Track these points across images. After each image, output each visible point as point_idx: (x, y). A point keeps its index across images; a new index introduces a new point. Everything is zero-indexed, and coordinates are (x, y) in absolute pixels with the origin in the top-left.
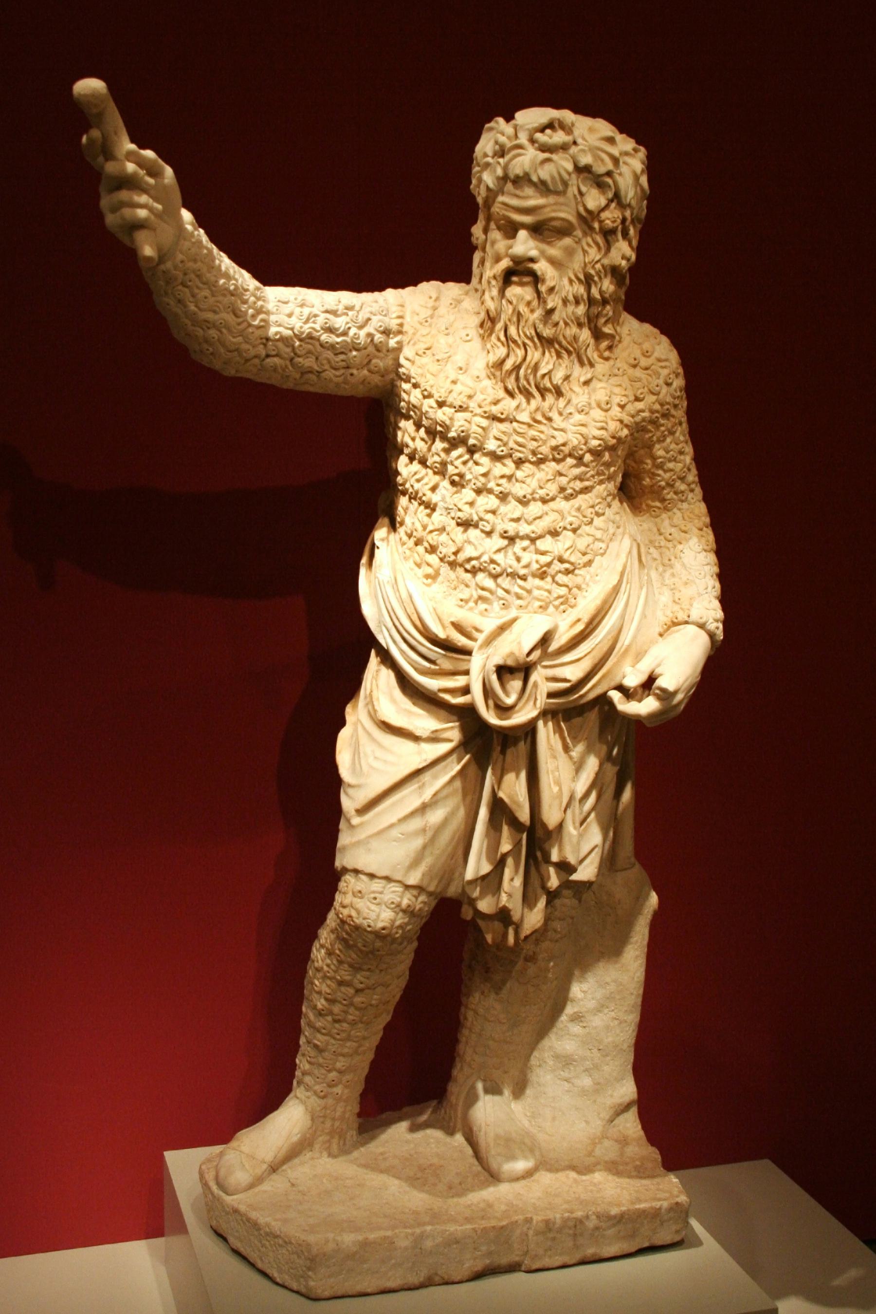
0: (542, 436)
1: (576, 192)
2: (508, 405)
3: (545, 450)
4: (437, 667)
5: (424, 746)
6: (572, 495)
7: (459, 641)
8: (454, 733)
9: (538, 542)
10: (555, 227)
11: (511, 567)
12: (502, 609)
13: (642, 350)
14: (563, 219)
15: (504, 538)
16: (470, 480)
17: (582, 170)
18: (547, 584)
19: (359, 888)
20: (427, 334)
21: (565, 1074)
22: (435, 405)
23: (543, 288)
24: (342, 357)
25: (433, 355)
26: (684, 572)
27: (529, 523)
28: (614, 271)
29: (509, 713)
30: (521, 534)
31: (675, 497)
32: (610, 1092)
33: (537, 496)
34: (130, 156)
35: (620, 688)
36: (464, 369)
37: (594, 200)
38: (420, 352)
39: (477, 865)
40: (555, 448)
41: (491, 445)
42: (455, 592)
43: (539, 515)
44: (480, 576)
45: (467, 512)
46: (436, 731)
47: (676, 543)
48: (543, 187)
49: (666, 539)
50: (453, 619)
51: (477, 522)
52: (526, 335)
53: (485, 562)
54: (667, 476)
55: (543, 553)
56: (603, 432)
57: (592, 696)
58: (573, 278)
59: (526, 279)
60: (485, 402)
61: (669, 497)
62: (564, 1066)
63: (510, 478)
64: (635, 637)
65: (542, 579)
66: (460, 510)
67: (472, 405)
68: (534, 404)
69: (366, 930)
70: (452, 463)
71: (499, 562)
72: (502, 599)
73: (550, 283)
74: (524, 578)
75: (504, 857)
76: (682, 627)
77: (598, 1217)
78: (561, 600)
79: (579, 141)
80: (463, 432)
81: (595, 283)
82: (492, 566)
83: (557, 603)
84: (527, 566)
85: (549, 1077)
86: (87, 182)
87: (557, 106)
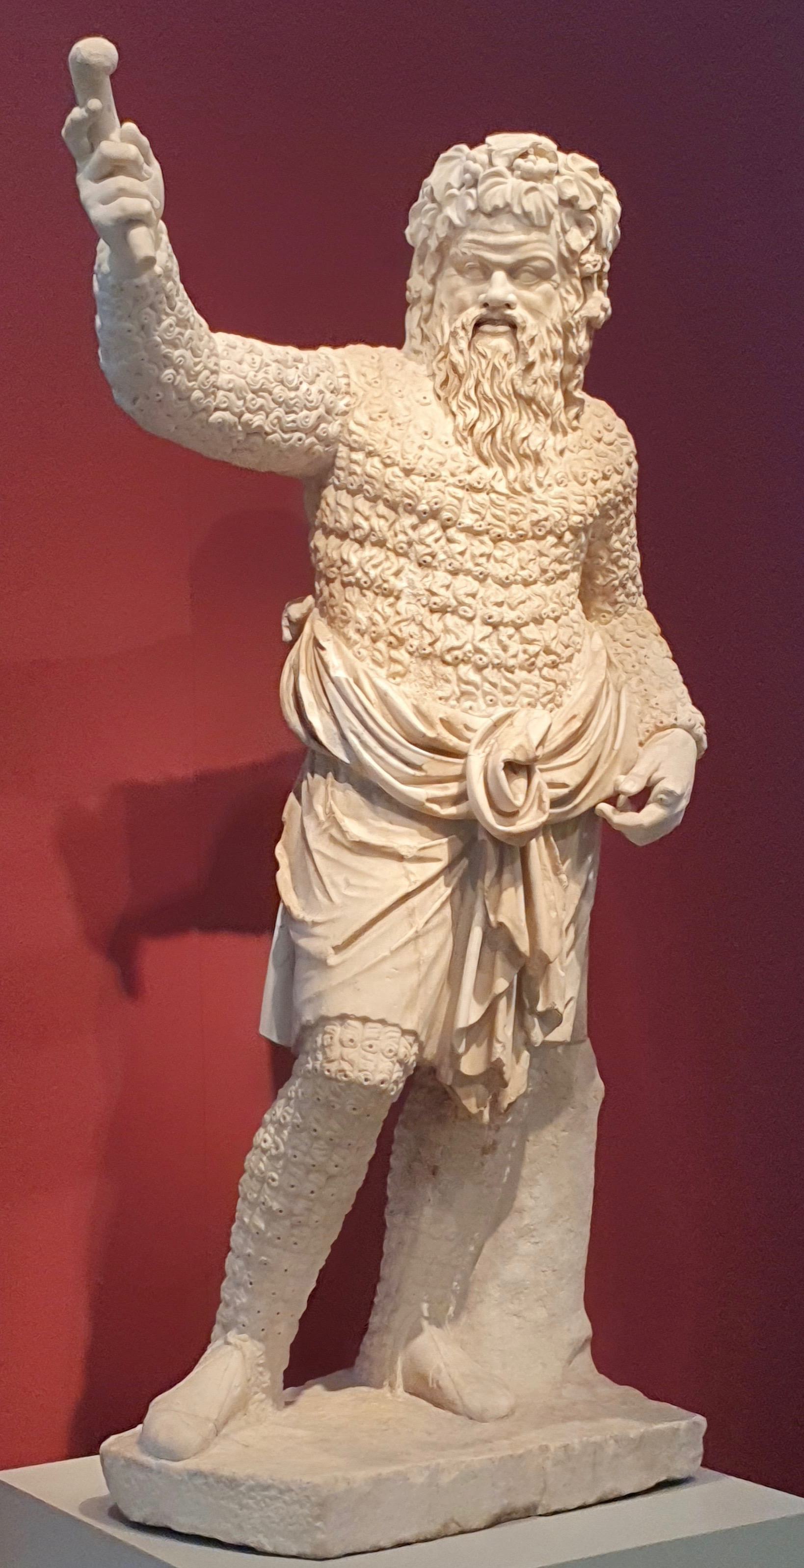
0: (523, 509)
1: (559, 229)
2: (484, 473)
3: (526, 525)
4: (423, 774)
5: (413, 867)
6: (553, 578)
7: (451, 740)
8: (441, 849)
9: (524, 630)
10: (536, 268)
11: (497, 657)
12: (488, 706)
13: (604, 423)
16: (443, 561)
17: (568, 203)
18: (535, 676)
19: (350, 1037)
20: (380, 396)
22: (401, 474)
24: (293, 416)
25: (391, 418)
27: (512, 608)
28: (590, 323)
29: (512, 820)
30: (505, 620)
31: (626, 599)
33: (518, 578)
34: (123, 140)
35: (612, 800)
36: (429, 433)
37: (577, 239)
38: (375, 416)
39: (470, 1012)
41: (468, 519)
42: (431, 690)
43: (523, 598)
44: (463, 669)
45: (445, 597)
46: (424, 848)
47: (637, 648)
48: (527, 221)
49: (623, 645)
50: (442, 715)
51: (456, 607)
53: (470, 652)
54: (621, 573)
55: (531, 642)
56: (583, 507)
57: (584, 808)
58: (551, 328)
63: (489, 556)
65: (530, 672)
66: (433, 594)
67: (445, 473)
68: (512, 473)
69: (361, 1085)
70: (422, 542)
71: (486, 650)
73: (531, 331)
74: (510, 670)
75: (498, 997)
78: (549, 697)
79: (563, 170)
80: (436, 504)
81: (573, 334)
82: (478, 656)
83: (545, 700)
84: (515, 656)
86: (56, 168)
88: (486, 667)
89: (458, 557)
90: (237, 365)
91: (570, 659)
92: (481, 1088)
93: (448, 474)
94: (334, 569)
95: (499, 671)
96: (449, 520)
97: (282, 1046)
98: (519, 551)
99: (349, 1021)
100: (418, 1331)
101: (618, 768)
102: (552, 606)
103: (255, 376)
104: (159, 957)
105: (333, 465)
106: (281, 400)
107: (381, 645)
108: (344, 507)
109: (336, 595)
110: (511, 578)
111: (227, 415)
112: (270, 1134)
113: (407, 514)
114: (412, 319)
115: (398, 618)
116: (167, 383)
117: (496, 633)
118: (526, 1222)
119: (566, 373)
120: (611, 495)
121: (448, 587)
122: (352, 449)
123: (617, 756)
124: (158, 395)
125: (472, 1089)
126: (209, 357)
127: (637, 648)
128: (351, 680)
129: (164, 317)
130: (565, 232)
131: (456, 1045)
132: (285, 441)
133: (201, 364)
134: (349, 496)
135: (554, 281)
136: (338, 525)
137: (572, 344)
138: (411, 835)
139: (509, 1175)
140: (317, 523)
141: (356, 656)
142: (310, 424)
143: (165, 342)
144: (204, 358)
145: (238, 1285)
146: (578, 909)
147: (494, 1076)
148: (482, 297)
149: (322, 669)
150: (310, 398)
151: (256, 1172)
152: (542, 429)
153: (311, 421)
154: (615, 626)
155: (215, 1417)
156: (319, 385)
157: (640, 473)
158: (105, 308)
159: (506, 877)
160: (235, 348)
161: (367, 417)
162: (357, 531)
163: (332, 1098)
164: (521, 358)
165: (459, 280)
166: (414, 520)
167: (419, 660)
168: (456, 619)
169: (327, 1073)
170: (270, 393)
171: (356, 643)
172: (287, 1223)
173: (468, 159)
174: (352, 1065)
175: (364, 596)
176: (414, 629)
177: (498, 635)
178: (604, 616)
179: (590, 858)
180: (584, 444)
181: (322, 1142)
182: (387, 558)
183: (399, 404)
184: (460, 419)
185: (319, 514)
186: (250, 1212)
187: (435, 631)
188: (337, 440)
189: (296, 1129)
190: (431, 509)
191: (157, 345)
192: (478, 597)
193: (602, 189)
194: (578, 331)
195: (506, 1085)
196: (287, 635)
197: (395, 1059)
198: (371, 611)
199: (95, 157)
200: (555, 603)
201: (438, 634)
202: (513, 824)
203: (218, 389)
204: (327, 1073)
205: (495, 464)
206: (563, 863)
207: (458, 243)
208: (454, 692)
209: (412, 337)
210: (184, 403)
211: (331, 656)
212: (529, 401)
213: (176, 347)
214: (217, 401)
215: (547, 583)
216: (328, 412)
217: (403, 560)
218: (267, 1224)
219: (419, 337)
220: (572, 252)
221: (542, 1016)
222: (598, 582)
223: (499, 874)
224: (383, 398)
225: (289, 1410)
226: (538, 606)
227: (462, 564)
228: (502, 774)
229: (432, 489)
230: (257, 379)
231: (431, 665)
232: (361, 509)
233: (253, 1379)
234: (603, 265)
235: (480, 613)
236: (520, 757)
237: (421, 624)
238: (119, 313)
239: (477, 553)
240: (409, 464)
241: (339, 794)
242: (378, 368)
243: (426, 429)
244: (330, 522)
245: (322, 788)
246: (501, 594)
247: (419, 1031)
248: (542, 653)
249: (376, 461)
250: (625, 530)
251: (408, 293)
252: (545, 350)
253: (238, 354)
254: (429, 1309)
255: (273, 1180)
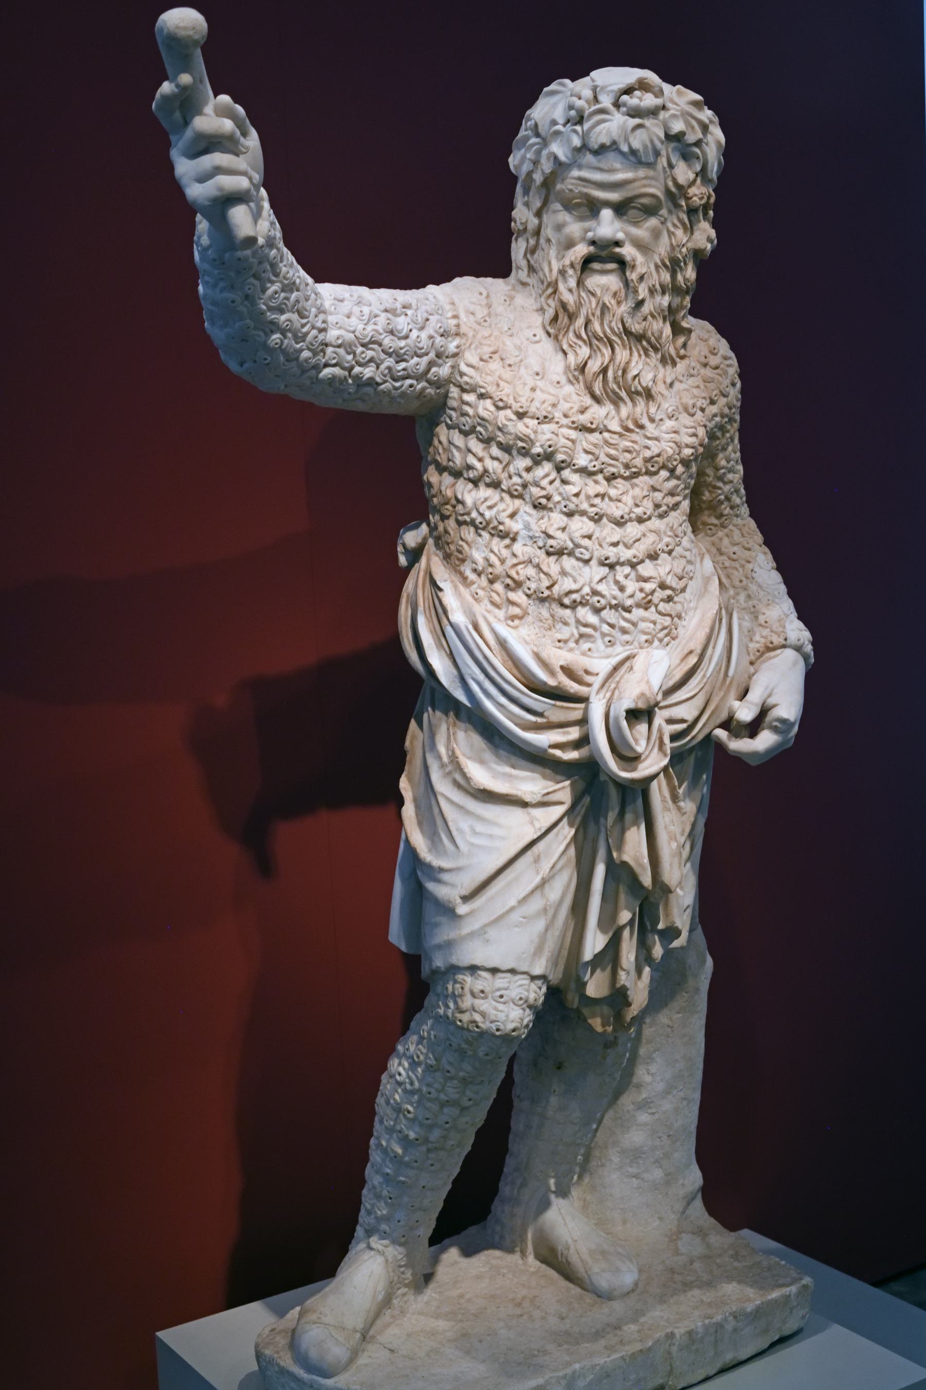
0: (636, 447)
1: (665, 165)
2: (599, 413)
5: (537, 812)
8: (564, 791)
9: (639, 567)
10: (642, 205)
11: (615, 598)
12: (607, 646)
13: (709, 347)
14: (653, 196)
15: (604, 565)
16: (559, 502)
18: (651, 613)
19: (481, 988)
20: (490, 336)
21: (633, 1170)
22: (514, 417)
23: (633, 276)
24: (403, 365)
25: (502, 359)
26: (762, 593)
27: (628, 547)
28: (697, 254)
29: (634, 764)
30: (622, 560)
31: (731, 512)
32: (681, 1182)
34: (217, 114)
35: (727, 725)
37: (684, 173)
38: (486, 357)
39: (594, 942)
40: (647, 460)
41: (582, 460)
42: (549, 633)
45: (561, 539)
46: (548, 794)
47: (743, 562)
48: (634, 157)
49: (729, 558)
50: (562, 663)
52: (612, 329)
53: (588, 595)
54: (727, 488)
55: (646, 580)
57: (701, 737)
58: (660, 264)
59: (613, 266)
60: (572, 411)
61: (726, 512)
62: (631, 1161)
63: (603, 496)
64: (735, 671)
65: (646, 609)
66: (550, 537)
67: (558, 415)
68: (624, 411)
69: (493, 1035)
70: (537, 485)
71: (604, 593)
72: (609, 635)
73: (641, 270)
74: (628, 610)
76: (779, 651)
77: (735, 1317)
78: (665, 632)
79: (669, 105)
80: (550, 446)
82: (596, 599)
83: (661, 635)
84: (632, 596)
85: (615, 1176)
86: (150, 144)
87: (642, 67)
88: (604, 608)
89: (574, 499)
90: (346, 319)
91: (683, 590)
92: (606, 1010)
93: (561, 415)
94: (448, 507)
95: (617, 610)
96: (563, 462)
97: (411, 955)
98: (633, 488)
99: (480, 973)
100: (545, 1205)
101: (733, 694)
102: (666, 540)
103: (364, 329)
104: (291, 837)
105: (445, 404)
106: (391, 350)
107: (498, 586)
108: (457, 447)
109: (452, 532)
110: (626, 517)
111: (337, 371)
112: (404, 1069)
113: (521, 457)
114: (518, 249)
115: (515, 561)
116: (275, 349)
117: (612, 573)
118: (644, 1096)
119: (674, 305)
120: (718, 419)
121: (564, 529)
122: (463, 390)
123: (731, 683)
124: (266, 359)
125: (597, 1009)
126: (316, 316)
127: (743, 562)
128: (470, 627)
129: (269, 285)
130: (671, 166)
131: (582, 975)
132: (396, 389)
133: (309, 325)
134: (462, 436)
135: (661, 216)
136: (451, 463)
137: (680, 277)
138: (533, 779)
139: (628, 1059)
140: (429, 458)
141: (473, 597)
142: (421, 371)
143: (270, 309)
144: (310, 319)
145: (378, 1197)
146: (694, 825)
147: (618, 998)
148: (590, 235)
149: (440, 610)
150: (421, 345)
151: (392, 1101)
152: (652, 365)
153: (422, 368)
154: (721, 539)
155: (362, 1326)
156: (429, 330)
157: (743, 391)
158: (207, 278)
159: (629, 817)
160: (342, 301)
161: (478, 359)
162: (470, 472)
163: (464, 1046)
164: (631, 296)
165: (564, 216)
166: (528, 462)
167: (537, 602)
168: (573, 561)
169: (459, 1023)
170: (380, 345)
171: (473, 583)
172: (424, 1148)
173: (571, 95)
174: (484, 1017)
175: (480, 535)
176: (531, 571)
177: (615, 575)
178: (710, 529)
179: (704, 777)
180: (692, 371)
181: (455, 1082)
182: (502, 499)
183: (509, 342)
184: (571, 357)
185: (431, 450)
186: (387, 1136)
187: (552, 574)
188: (449, 381)
189: (429, 1069)
190: (545, 452)
191: (263, 313)
192: (594, 538)
193: (707, 121)
194: (685, 264)
195: (629, 1005)
196: (403, 560)
197: (525, 1006)
198: (487, 552)
199: (189, 134)
200: (670, 536)
201: (555, 578)
202: (634, 769)
203: (327, 345)
204: (459, 1023)
205: (608, 403)
206: (680, 787)
207: (563, 180)
208: (573, 635)
209: (518, 268)
210: (294, 364)
211: (449, 598)
212: (639, 338)
213: (282, 312)
214: (326, 358)
215: (661, 516)
216: (438, 355)
217: (518, 502)
218: (405, 1149)
219: (526, 270)
220: (679, 187)
221: (662, 933)
222: (704, 498)
223: (622, 814)
224: (492, 338)
225: (430, 1293)
226: (653, 543)
227: (577, 506)
228: (624, 723)
229: (546, 431)
230: (366, 332)
231: (549, 608)
232: (474, 450)
233: (396, 1279)
234: (709, 198)
235: (596, 554)
236: (641, 705)
237: (538, 567)
238: (222, 284)
239: (592, 492)
240: (521, 407)
241: (461, 735)
242: (487, 304)
243: (537, 369)
244: (442, 459)
245: (444, 727)
246: (616, 534)
247: (547, 974)
248: (658, 589)
249: (488, 403)
250: (730, 448)
251: (513, 224)
252: (654, 286)
253: (346, 307)
254: (556, 1184)
255: (409, 1112)
